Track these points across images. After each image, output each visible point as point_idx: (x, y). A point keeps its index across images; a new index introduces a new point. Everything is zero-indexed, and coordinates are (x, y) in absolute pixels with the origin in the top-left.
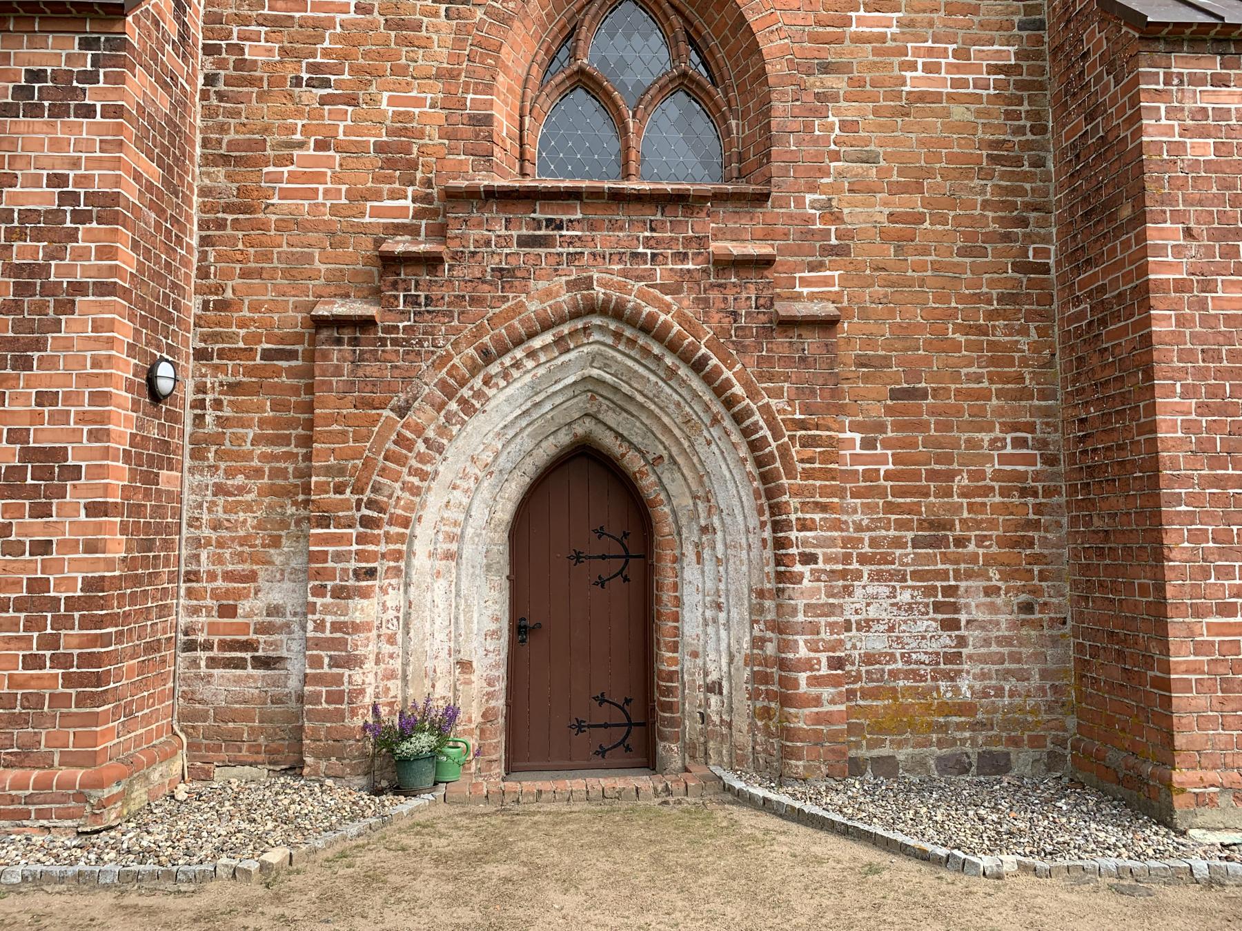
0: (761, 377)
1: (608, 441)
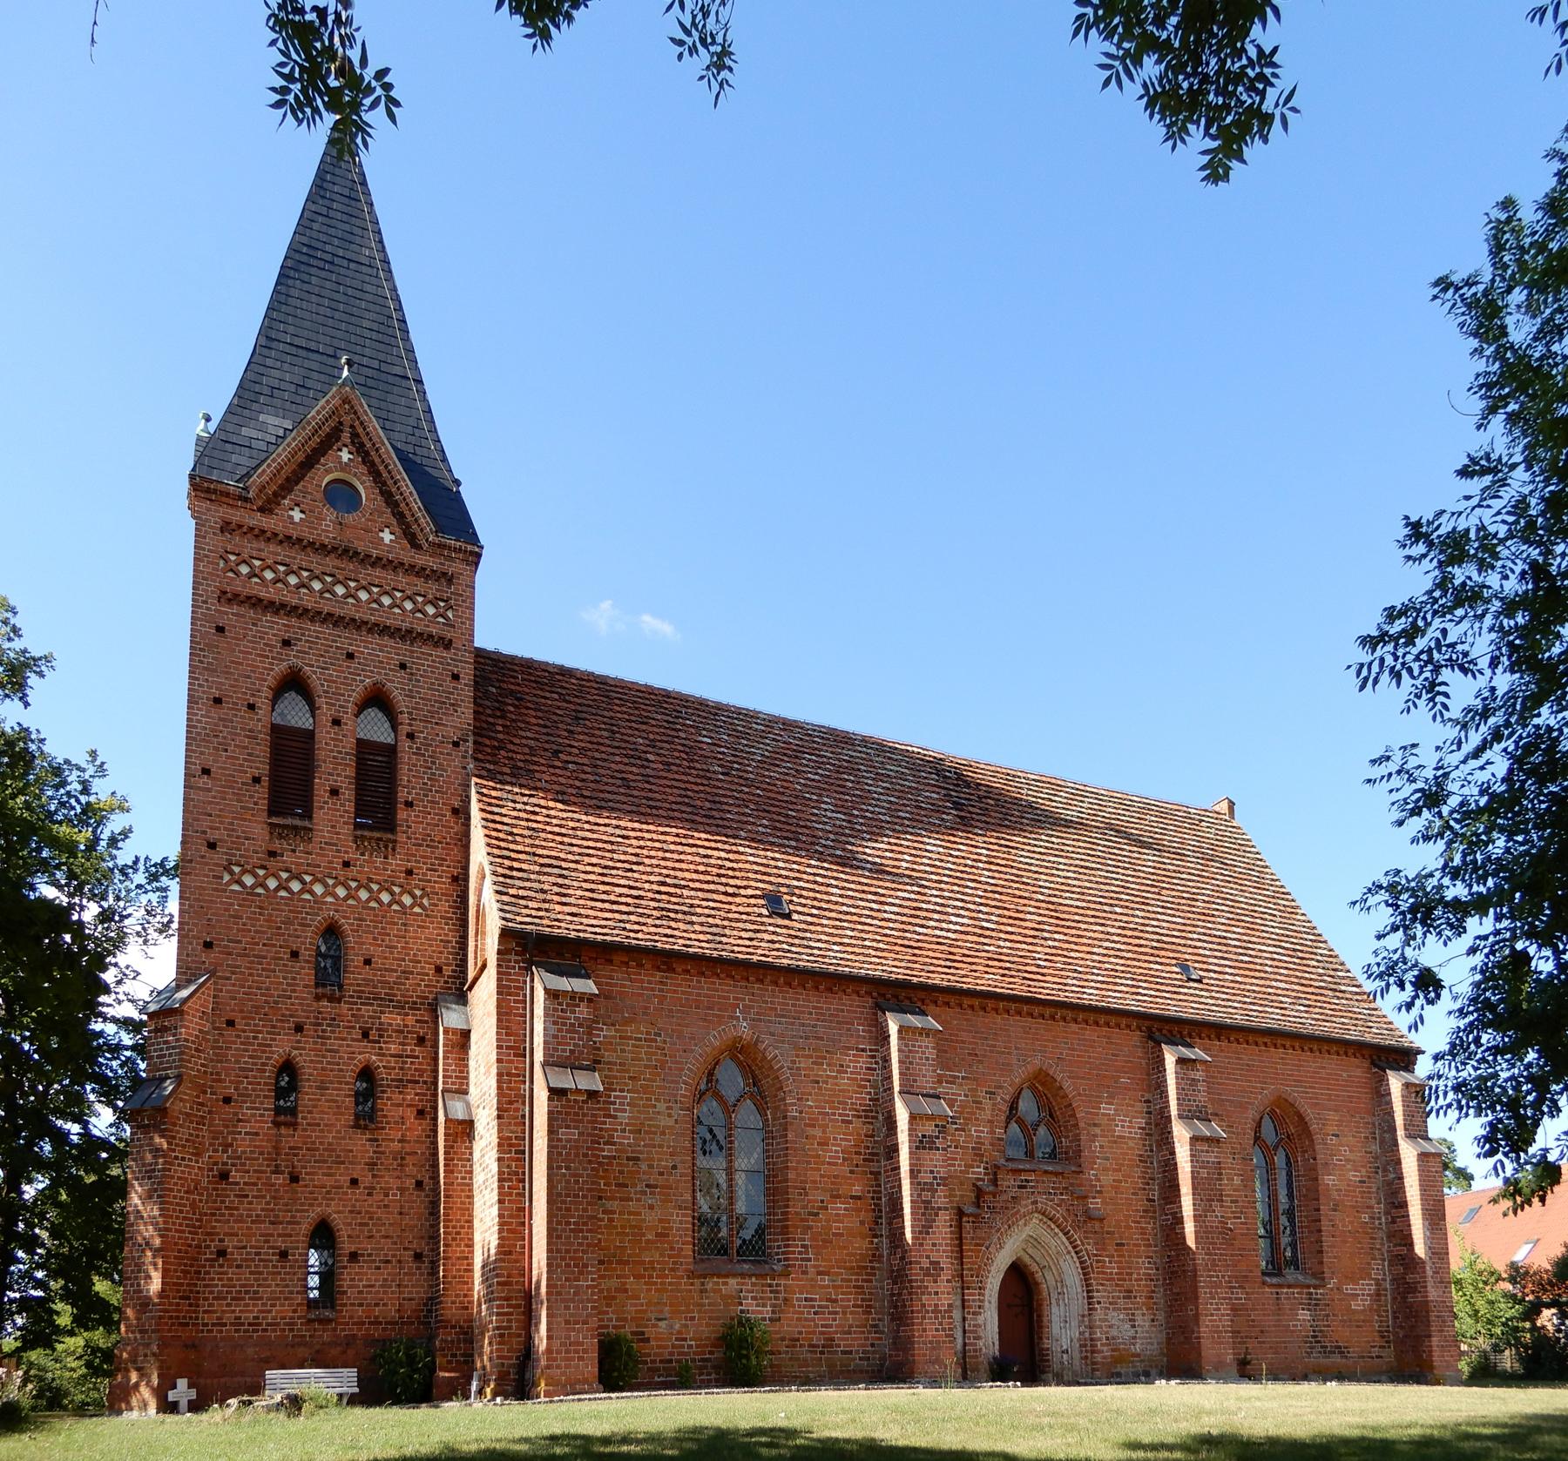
0: (1087, 1238)
1: (1027, 1260)
